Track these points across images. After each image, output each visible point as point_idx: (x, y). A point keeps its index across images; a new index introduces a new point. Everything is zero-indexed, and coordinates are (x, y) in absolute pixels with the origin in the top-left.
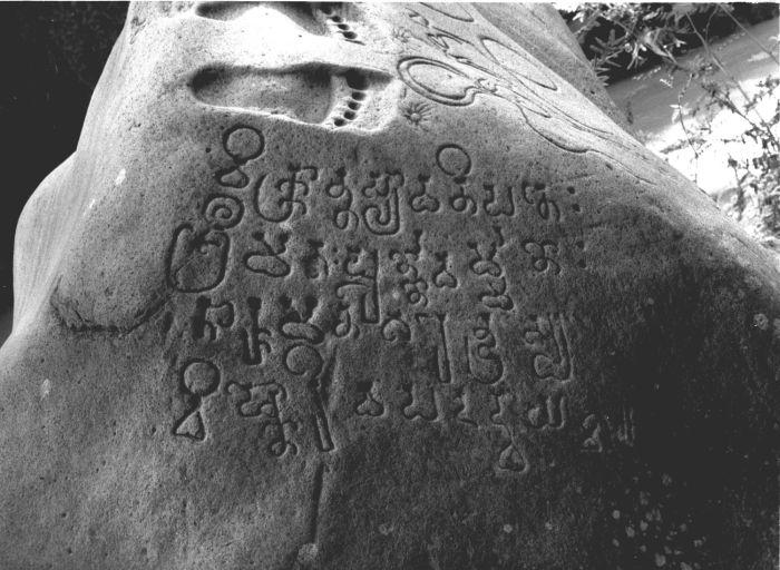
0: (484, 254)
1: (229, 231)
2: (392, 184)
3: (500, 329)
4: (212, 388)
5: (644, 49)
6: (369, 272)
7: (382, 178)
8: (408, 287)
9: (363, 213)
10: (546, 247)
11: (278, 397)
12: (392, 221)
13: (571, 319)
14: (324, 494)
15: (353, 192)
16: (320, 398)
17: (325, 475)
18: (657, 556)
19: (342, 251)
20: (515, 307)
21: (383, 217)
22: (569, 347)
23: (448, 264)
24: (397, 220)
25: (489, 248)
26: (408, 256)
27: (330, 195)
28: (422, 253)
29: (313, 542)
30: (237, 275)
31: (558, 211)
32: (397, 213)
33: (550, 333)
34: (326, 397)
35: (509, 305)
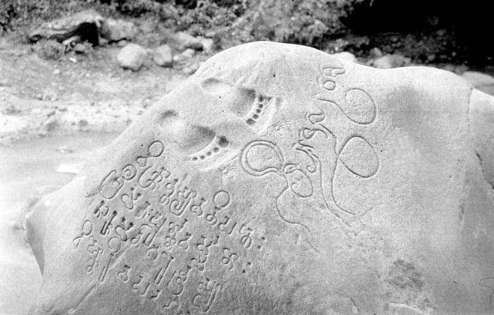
0: (205, 244)
1: (125, 181)
2: (190, 196)
3: (191, 276)
4: (87, 235)
5: (89, 95)
6: (158, 226)
7: (189, 191)
8: (168, 239)
9: (172, 201)
10: (233, 256)
11: (100, 252)
12: (180, 211)
13: (223, 290)
14: (89, 295)
15: (175, 191)
16: (111, 261)
17: (93, 290)
18: (346, 16)
19: (154, 212)
20: (203, 272)
21: (178, 207)
22: (214, 300)
23: (189, 239)
24: (182, 212)
25: (209, 243)
26: (176, 227)
27: (121, 198)
28: (182, 229)
29: (75, 309)
30: (116, 201)
31: (250, 244)
32: (265, 173)
33: (211, 290)
34: (113, 262)
35: (202, 269)
